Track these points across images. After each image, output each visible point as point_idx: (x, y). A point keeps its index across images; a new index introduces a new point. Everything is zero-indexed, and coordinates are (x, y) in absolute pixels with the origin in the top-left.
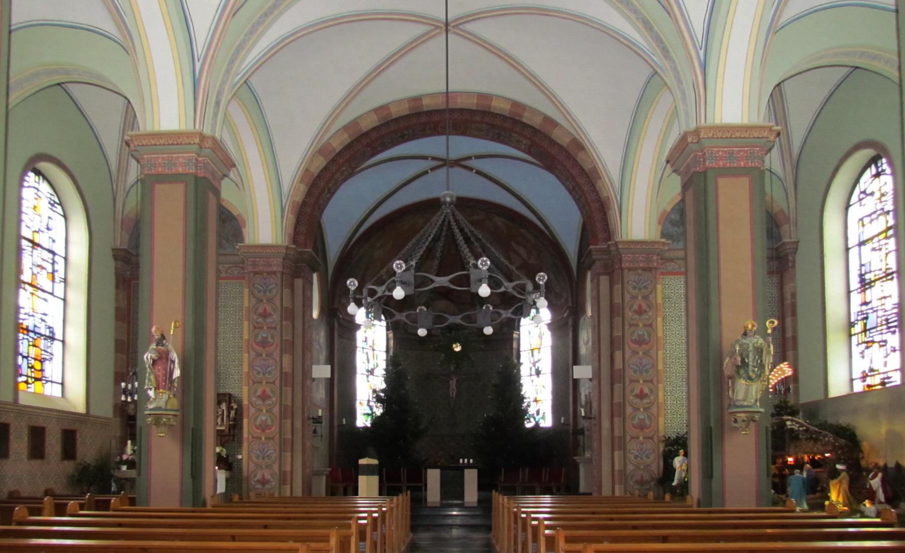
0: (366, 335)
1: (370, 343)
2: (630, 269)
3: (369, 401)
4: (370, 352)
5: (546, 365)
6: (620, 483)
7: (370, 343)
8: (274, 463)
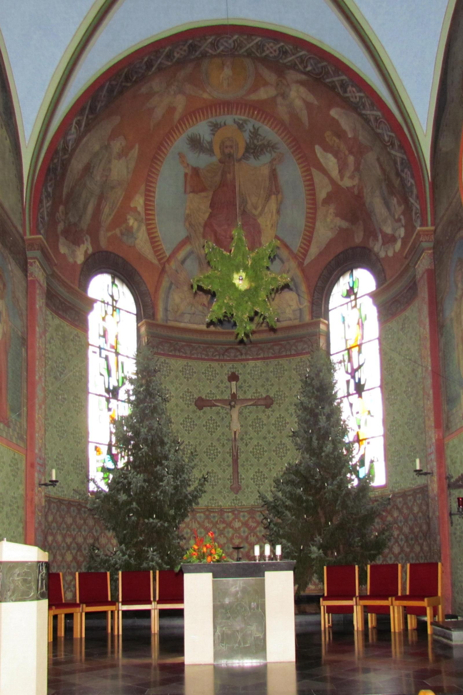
0: (106, 325)
1: (112, 340)
3: (110, 446)
4: (112, 357)
5: (372, 374)
6: (61, 637)
7: (112, 340)
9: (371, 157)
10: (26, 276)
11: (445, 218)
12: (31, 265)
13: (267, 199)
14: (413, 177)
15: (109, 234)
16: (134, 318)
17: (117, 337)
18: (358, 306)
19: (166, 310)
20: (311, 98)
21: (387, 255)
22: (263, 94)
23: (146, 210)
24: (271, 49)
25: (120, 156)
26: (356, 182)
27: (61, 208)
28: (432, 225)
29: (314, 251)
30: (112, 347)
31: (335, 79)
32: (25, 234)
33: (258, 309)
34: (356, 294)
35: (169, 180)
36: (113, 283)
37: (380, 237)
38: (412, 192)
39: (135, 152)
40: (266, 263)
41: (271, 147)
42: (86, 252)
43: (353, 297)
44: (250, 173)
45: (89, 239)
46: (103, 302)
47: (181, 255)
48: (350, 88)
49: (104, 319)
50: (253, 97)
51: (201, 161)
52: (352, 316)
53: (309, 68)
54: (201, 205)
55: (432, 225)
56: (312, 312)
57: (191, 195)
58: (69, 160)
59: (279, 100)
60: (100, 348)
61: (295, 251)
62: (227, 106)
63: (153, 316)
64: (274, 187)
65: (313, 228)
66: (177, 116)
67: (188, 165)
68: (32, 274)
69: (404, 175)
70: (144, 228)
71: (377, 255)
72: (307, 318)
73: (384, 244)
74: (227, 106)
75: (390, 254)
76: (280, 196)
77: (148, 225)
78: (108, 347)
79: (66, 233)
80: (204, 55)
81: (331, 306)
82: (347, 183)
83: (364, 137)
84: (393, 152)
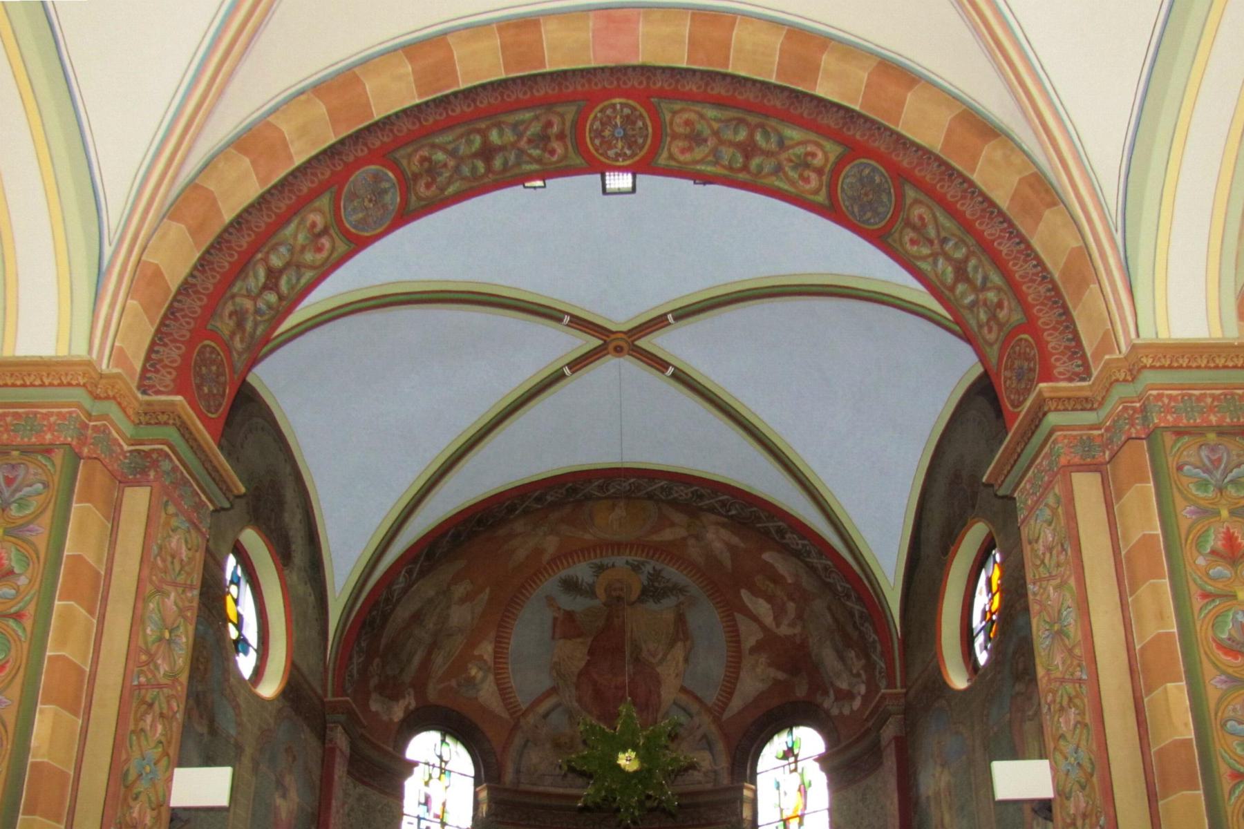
1: (436, 808)
2: (1179, 433)
7: (436, 808)
8: (37, 515)
9: (819, 605)
10: (324, 743)
11: (920, 682)
12: (331, 730)
13: (672, 644)
14: (876, 632)
15: (441, 686)
16: (472, 781)
17: (444, 804)
18: (799, 770)
19: (518, 771)
20: (735, 540)
21: (841, 713)
22: (667, 535)
23: (495, 663)
24: (681, 492)
25: (462, 601)
26: (798, 630)
27: (377, 660)
28: (904, 686)
29: (736, 704)
30: (437, 816)
31: (770, 524)
32: (326, 696)
33: (651, 793)
34: (796, 756)
35: (530, 630)
36: (443, 741)
37: (832, 692)
38: (875, 648)
39: (485, 595)
40: (664, 740)
41: (676, 589)
42: (407, 708)
43: (792, 759)
44: (646, 623)
45: (412, 692)
46: (427, 764)
47: (542, 709)
48: (788, 536)
49: (427, 784)
50: (656, 538)
51: (577, 604)
52: (791, 782)
53: (733, 512)
54: (576, 653)
55: (902, 687)
56: (732, 773)
57: (562, 641)
58: (393, 610)
59: (691, 542)
60: (419, 818)
61: (710, 704)
62: (617, 547)
63: (499, 778)
64: (680, 631)
65: (737, 678)
66: (546, 557)
67: (559, 609)
68: (331, 741)
69: (863, 629)
70: (491, 677)
71: (827, 712)
72: (725, 781)
73: (837, 699)
74: (617, 547)
75: (846, 711)
76: (688, 643)
77: (496, 674)
78: (431, 817)
79: (381, 688)
80: (588, 497)
81: (759, 769)
82: (784, 630)
83: (808, 583)
84: (848, 603)
